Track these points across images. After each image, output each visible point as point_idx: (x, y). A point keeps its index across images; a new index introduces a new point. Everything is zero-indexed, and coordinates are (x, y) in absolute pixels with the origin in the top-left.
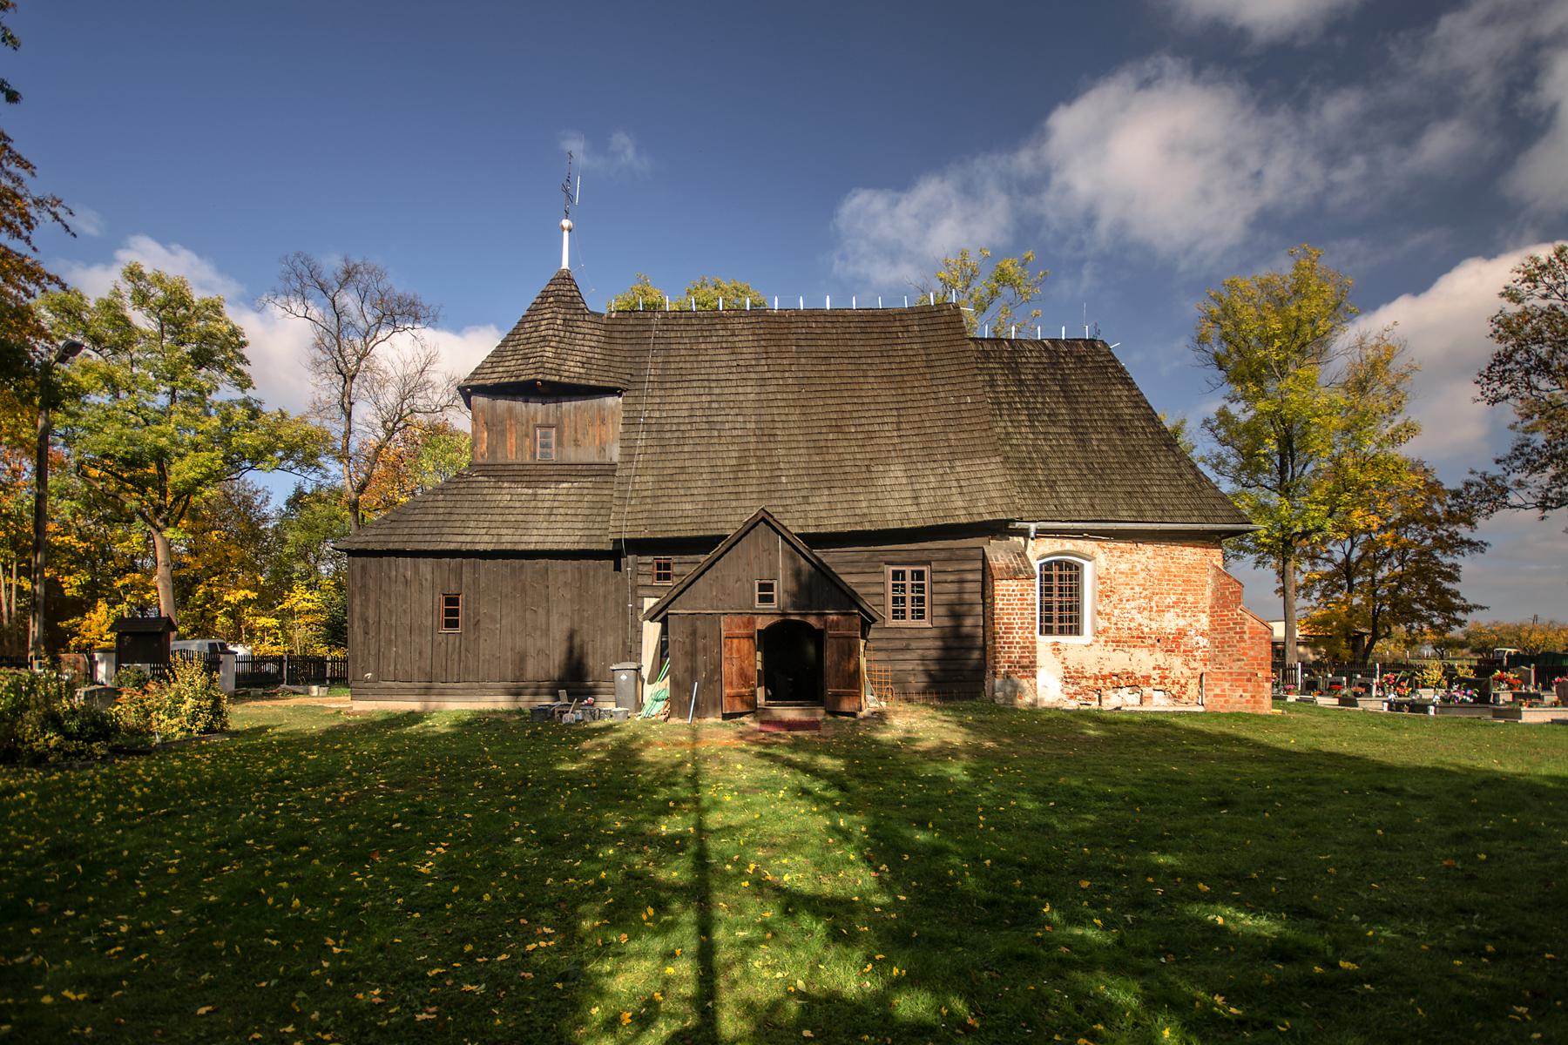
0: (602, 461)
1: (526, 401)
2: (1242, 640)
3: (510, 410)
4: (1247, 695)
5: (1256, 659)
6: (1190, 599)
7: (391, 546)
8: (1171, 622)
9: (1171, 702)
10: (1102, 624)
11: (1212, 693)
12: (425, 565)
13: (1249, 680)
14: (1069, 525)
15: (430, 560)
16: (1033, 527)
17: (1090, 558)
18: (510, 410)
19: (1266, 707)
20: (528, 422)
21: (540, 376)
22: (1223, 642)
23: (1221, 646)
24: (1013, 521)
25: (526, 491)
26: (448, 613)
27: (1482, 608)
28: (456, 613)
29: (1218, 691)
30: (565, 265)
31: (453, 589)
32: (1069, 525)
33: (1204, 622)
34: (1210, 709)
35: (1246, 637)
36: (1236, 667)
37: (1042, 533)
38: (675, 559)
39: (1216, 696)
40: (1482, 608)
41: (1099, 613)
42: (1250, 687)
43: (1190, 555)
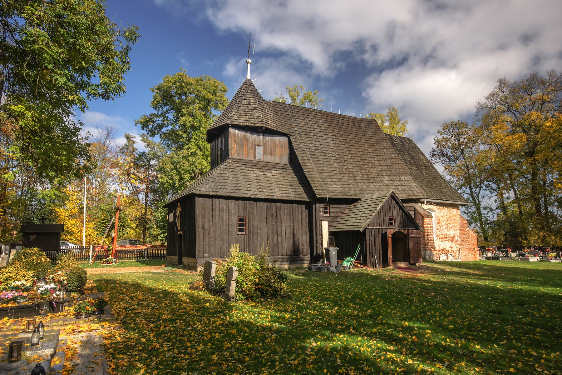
0: (282, 163)
1: (252, 134)
2: (469, 238)
3: (245, 136)
4: (473, 256)
5: (473, 244)
6: (455, 225)
7: (220, 194)
8: (452, 233)
9: (453, 258)
10: (438, 233)
11: (463, 255)
12: (232, 203)
13: (473, 251)
14: (433, 201)
15: (233, 201)
16: (426, 200)
17: (434, 211)
18: (245, 136)
19: (479, 258)
20: (252, 142)
21: (265, 125)
22: (464, 239)
23: (463, 240)
24: (422, 198)
25: (260, 173)
26: (240, 225)
27: (294, 236)
28: (243, 225)
29: (464, 254)
30: (249, 78)
31: (241, 214)
32: (433, 201)
33: (458, 233)
34: (463, 260)
35: (470, 237)
36: (468, 246)
37: (428, 203)
38: (331, 206)
39: (464, 256)
40: (294, 236)
41: (437, 229)
42: (473, 252)
43: (454, 211)
